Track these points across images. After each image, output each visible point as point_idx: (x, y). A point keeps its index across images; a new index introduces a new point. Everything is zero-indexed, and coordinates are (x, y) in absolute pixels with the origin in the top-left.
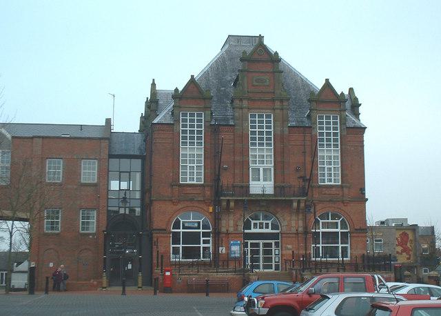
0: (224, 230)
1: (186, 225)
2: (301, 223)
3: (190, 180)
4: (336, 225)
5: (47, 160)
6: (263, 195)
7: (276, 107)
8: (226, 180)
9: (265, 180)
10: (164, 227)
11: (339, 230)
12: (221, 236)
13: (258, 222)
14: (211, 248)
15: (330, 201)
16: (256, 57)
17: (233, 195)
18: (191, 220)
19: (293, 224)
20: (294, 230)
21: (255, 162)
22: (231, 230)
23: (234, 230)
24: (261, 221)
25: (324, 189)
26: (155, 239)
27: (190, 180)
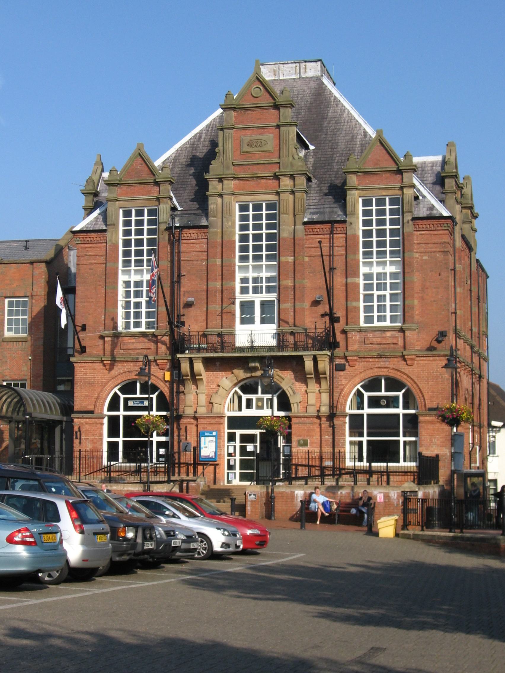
0: (189, 411)
1: (130, 403)
2: (325, 398)
3: (378, 321)
4: (392, 402)
5: (7, 301)
6: (252, 348)
7: (283, 188)
8: (193, 324)
9: (263, 321)
10: (91, 408)
11: (400, 411)
12: (183, 421)
13: (253, 397)
14: (397, 464)
15: (380, 357)
16: (250, 102)
17: (199, 350)
18: (138, 395)
19: (312, 398)
20: (312, 411)
21: (244, 290)
22: (202, 411)
23: (208, 413)
24: (260, 395)
25: (370, 335)
26: (76, 429)
27: (378, 321)
